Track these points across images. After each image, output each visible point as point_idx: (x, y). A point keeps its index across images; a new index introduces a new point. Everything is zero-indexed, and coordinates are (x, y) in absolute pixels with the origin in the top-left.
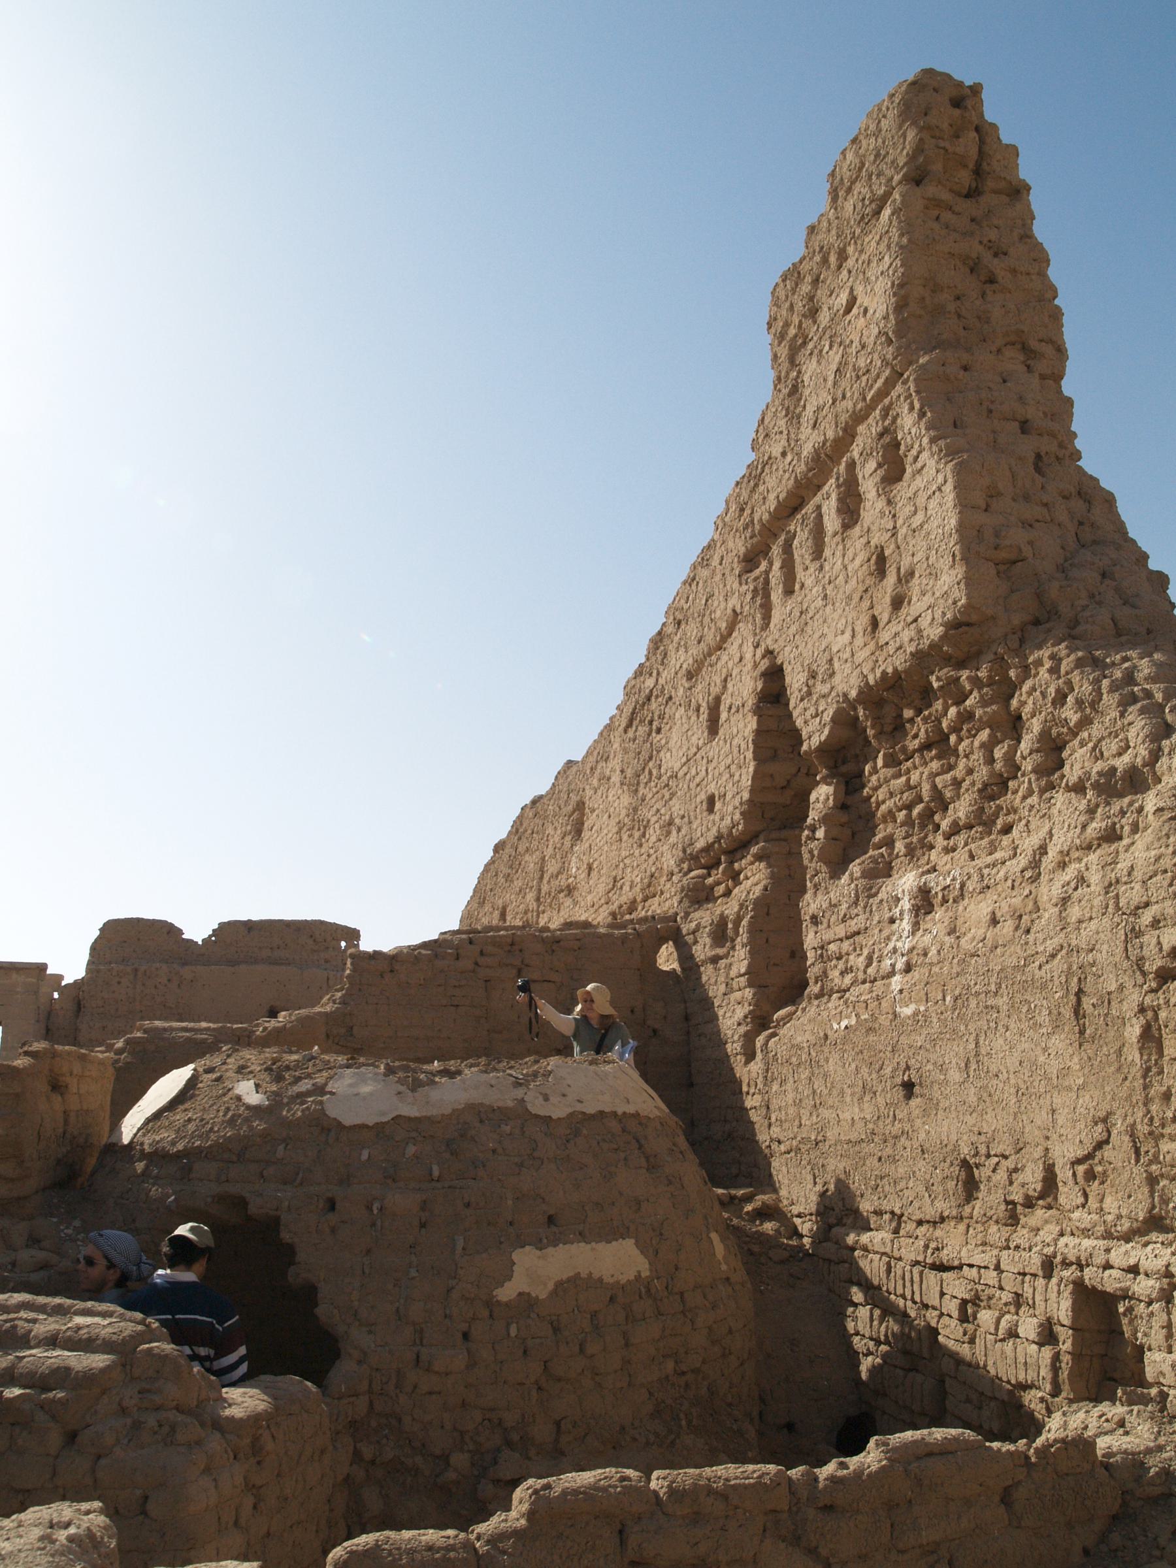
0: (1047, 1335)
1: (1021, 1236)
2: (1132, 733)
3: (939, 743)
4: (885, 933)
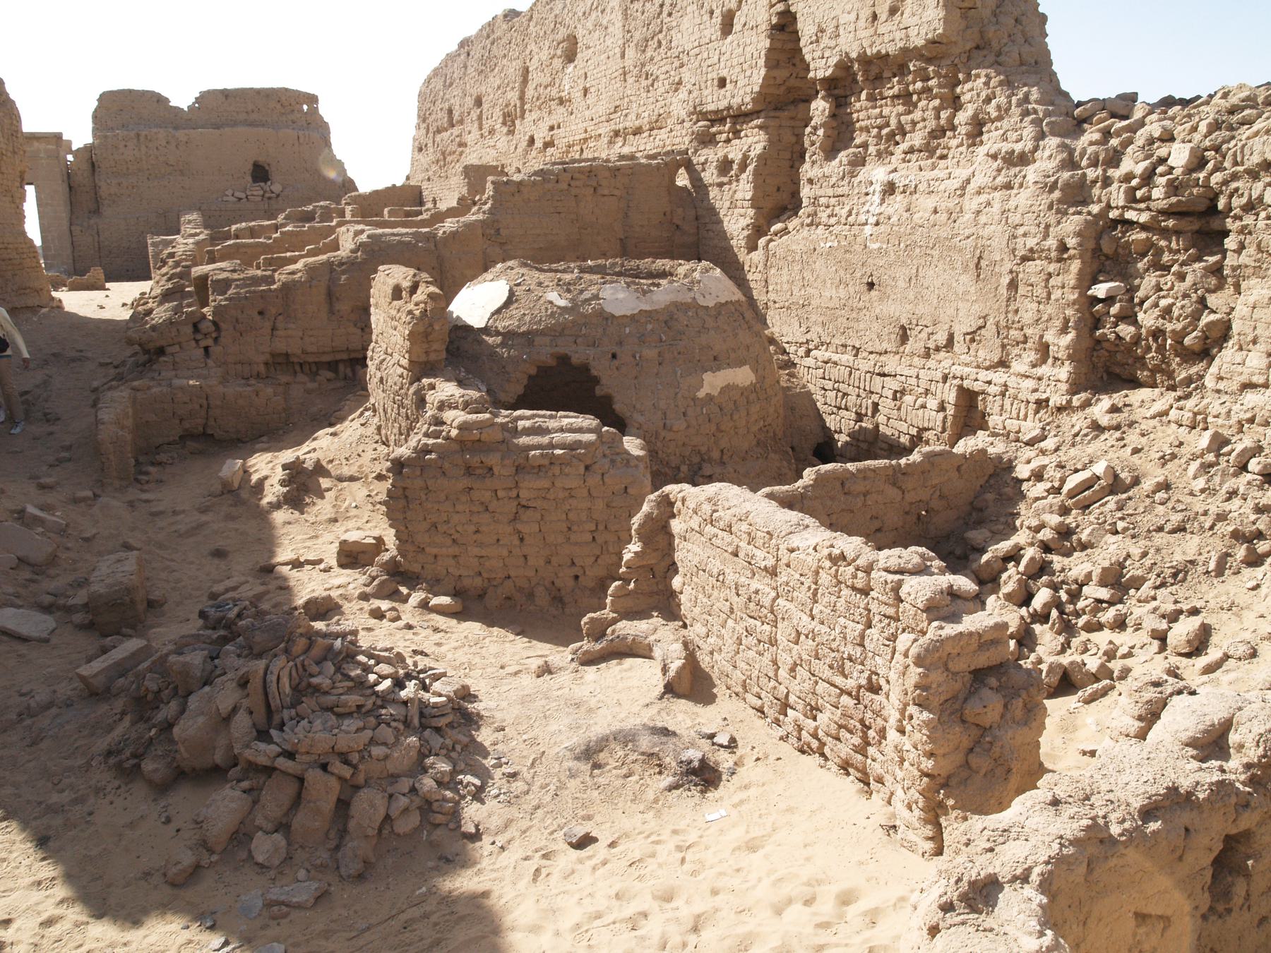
0: (942, 408)
1: (931, 363)
2: (1025, 133)
3: (905, 97)
4: (862, 200)
